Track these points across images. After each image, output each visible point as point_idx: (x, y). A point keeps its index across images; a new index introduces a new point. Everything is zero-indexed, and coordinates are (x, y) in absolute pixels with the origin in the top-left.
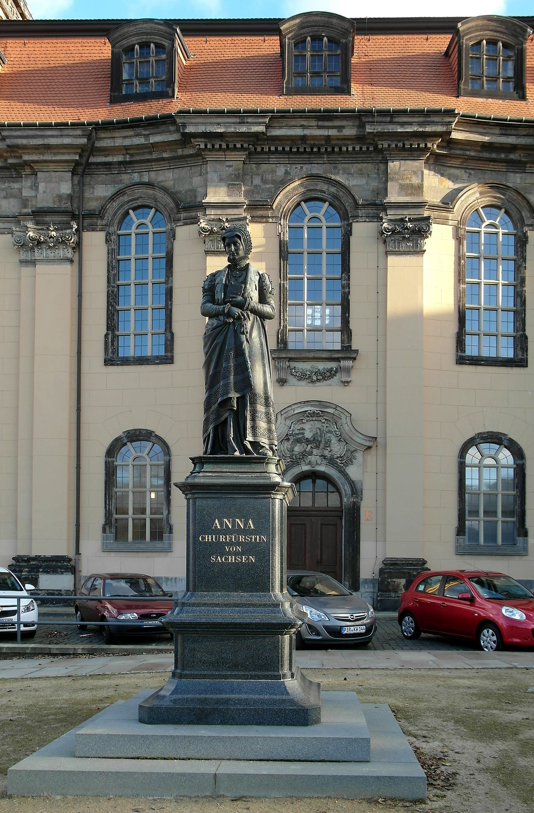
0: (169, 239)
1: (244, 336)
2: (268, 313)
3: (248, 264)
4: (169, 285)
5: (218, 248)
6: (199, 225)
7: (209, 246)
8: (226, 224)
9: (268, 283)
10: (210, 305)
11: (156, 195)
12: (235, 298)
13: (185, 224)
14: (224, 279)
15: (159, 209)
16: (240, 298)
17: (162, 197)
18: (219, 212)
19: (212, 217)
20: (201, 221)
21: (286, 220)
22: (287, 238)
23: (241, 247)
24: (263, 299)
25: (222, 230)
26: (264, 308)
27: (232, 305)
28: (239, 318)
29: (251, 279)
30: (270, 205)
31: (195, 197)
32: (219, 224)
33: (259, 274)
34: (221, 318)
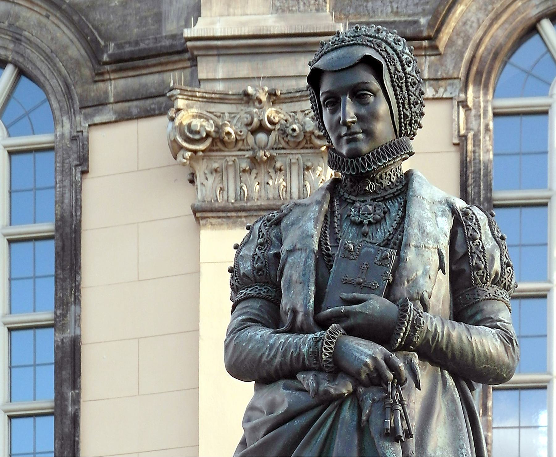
0: (65, 172)
1: (398, 447)
2: (489, 358)
3: (409, 175)
4: (69, 334)
5: (240, 196)
6: (172, 119)
7: (208, 189)
8: (270, 112)
9: (489, 243)
11: (17, 17)
12: (359, 301)
13: (124, 117)
15: (29, 67)
16: (377, 304)
17: (40, 25)
18: (243, 68)
19: (220, 87)
20: (181, 103)
21: (486, 87)
22: (486, 153)
23: (383, 108)
24: (465, 306)
25: (254, 132)
27: (350, 331)
28: (376, 379)
29: (423, 231)
30: (429, 38)
31: (159, 18)
32: (244, 113)
33: (454, 211)
34: (308, 380)
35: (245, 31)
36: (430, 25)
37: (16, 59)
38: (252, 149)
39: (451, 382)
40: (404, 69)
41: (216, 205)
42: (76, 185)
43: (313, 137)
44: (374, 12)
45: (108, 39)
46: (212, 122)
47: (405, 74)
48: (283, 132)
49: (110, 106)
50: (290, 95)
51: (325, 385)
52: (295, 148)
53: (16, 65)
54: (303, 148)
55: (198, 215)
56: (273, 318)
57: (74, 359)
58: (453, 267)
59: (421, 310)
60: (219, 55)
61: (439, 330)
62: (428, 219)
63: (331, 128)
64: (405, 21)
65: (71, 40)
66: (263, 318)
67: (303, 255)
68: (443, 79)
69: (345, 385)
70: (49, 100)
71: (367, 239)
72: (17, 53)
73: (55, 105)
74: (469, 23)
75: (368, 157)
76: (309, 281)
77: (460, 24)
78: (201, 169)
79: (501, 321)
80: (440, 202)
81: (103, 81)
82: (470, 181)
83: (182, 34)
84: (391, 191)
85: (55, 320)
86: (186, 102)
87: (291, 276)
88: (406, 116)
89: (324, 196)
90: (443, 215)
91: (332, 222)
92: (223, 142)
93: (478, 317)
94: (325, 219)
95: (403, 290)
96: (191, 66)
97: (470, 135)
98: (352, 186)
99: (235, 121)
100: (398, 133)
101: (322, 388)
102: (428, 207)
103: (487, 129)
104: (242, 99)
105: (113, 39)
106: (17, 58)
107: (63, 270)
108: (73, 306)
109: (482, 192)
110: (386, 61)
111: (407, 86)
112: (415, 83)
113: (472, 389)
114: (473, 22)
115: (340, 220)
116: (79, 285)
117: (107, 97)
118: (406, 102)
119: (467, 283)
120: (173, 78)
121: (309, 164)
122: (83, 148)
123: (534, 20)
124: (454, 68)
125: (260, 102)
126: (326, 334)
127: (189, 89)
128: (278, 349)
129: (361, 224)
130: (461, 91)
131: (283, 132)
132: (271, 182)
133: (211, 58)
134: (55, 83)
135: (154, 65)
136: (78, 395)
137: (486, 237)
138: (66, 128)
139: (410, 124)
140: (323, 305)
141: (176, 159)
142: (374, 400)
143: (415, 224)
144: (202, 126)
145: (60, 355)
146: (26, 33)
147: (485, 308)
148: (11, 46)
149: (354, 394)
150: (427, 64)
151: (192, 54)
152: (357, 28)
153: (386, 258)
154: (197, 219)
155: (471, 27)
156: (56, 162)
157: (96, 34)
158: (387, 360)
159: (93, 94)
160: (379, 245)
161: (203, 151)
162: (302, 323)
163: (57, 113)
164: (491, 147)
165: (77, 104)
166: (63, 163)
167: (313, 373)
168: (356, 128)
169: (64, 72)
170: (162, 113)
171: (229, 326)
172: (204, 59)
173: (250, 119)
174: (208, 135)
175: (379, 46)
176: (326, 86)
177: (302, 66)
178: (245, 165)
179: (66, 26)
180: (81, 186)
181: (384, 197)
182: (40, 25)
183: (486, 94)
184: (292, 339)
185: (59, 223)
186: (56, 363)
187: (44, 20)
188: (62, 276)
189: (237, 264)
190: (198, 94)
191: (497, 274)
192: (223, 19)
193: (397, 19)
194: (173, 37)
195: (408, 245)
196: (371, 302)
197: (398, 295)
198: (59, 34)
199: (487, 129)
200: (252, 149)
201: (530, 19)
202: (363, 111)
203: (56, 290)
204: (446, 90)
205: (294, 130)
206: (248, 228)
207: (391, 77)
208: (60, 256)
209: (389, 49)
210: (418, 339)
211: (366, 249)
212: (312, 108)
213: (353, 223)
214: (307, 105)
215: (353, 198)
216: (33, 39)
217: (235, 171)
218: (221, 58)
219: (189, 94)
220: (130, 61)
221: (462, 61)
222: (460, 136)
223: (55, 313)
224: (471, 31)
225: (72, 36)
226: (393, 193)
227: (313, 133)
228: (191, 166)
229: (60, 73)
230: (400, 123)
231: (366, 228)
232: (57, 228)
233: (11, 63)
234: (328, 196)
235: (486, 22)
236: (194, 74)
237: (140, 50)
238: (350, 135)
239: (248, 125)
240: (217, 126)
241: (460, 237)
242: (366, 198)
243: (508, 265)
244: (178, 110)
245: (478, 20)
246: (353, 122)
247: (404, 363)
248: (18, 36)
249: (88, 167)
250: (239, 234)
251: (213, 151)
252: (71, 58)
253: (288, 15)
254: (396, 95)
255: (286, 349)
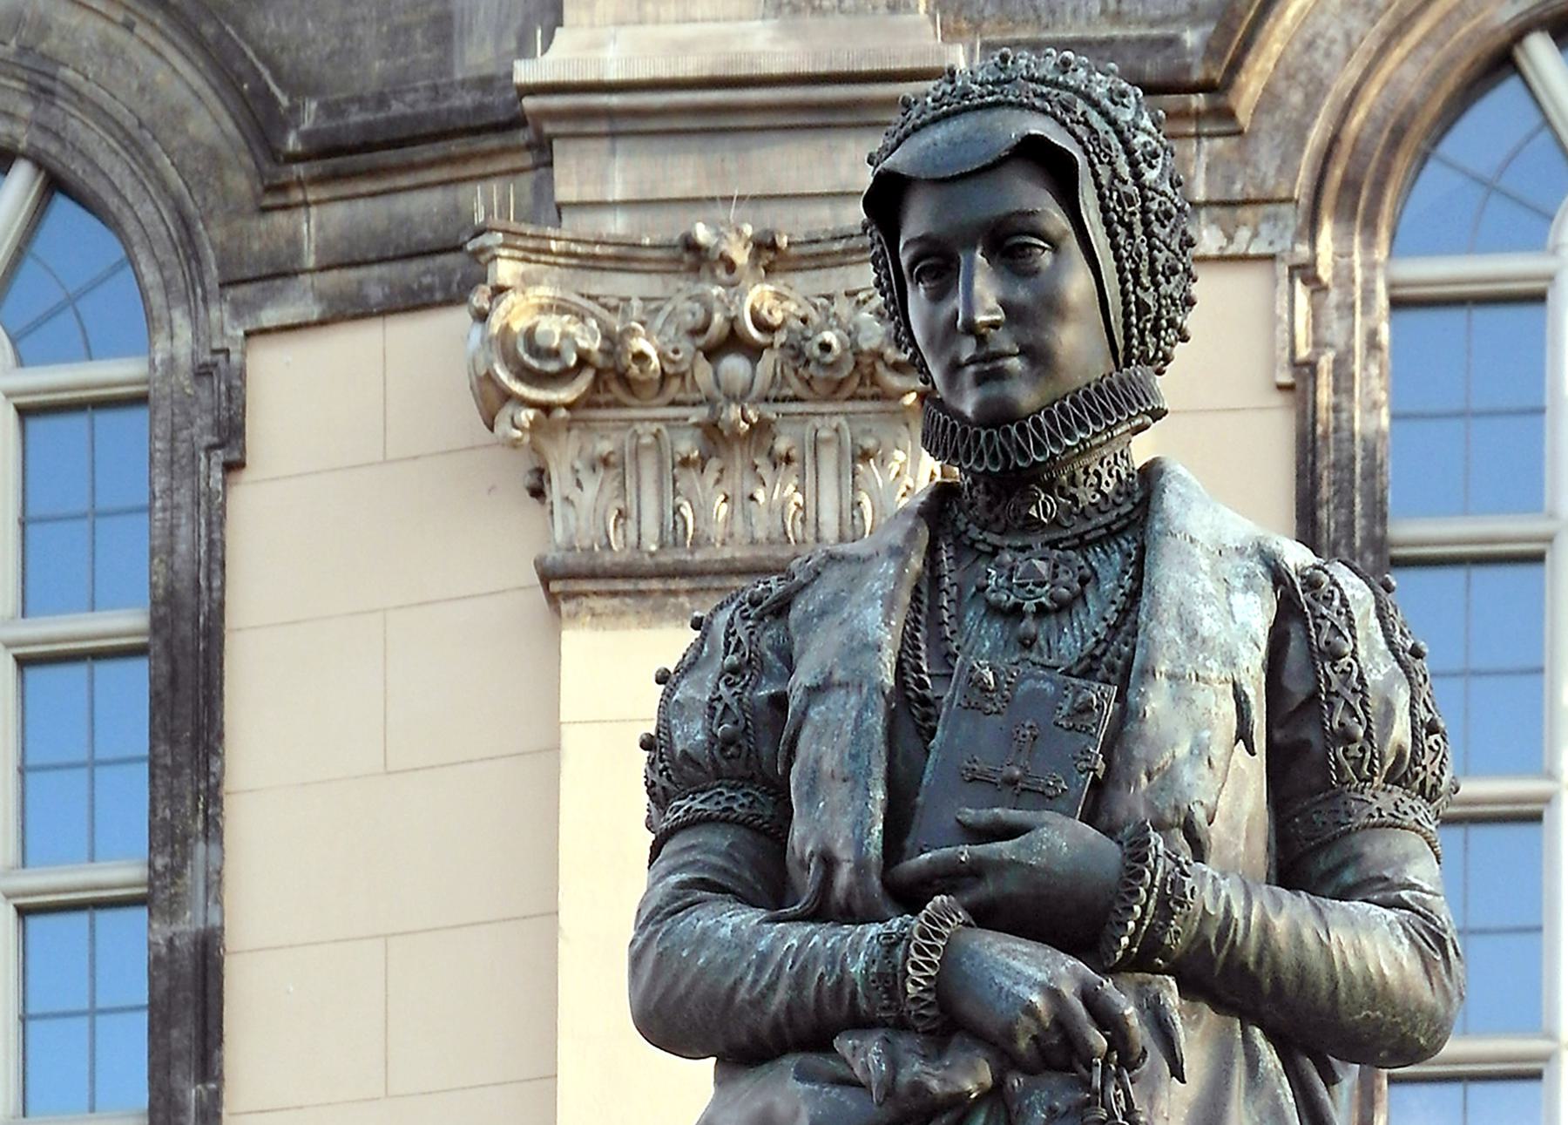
0: (179, 464)
2: (1378, 993)
3: (1151, 475)
4: (189, 923)
5: (672, 534)
6: (482, 316)
7: (583, 513)
9: (1379, 668)
10: (734, 921)
13: (346, 311)
14: (889, 639)
15: (76, 169)
16: (1061, 840)
17: (108, 51)
18: (681, 171)
19: (616, 225)
20: (506, 270)
21: (1370, 225)
23: (1077, 284)
24: (1311, 848)
25: (713, 353)
26: (1340, 937)
27: (986, 916)
28: (1059, 1051)
29: (1191, 634)
30: (1207, 87)
32: (684, 297)
33: (1278, 576)
34: (865, 1054)
35: (688, 67)
36: (1212, 51)
37: (40, 144)
38: (709, 401)
39: (1270, 1058)
40: (1137, 176)
41: (607, 559)
42: (210, 502)
43: (880, 367)
44: (1052, 12)
45: (300, 88)
46: (593, 323)
47: (1142, 187)
48: (796, 352)
49: (306, 280)
50: (815, 248)
51: (914, 1068)
52: (831, 397)
53: (39, 163)
54: (851, 398)
55: (555, 587)
56: (766, 878)
57: (205, 994)
58: (1278, 735)
59: (1186, 856)
60: (613, 135)
61: (1237, 913)
62: (1207, 599)
63: (930, 341)
64: (1141, 40)
65: (195, 93)
66: (739, 878)
67: (853, 699)
68: (1247, 202)
69: (971, 1069)
70: (132, 261)
71: (1034, 656)
72: (44, 128)
73: (151, 277)
74: (1322, 43)
75: (1036, 423)
76: (869, 774)
77: (1298, 46)
78: (563, 458)
79: (1412, 886)
80: (1240, 551)
81: (285, 207)
82: (1325, 491)
83: (510, 75)
84: (1102, 520)
85: (150, 884)
86: (522, 267)
87: (818, 761)
88: (1143, 308)
89: (911, 534)
90: (1247, 588)
91: (935, 607)
92: (624, 380)
93: (1349, 877)
94: (916, 598)
95: (1135, 799)
96: (536, 167)
97: (1325, 362)
98: (990, 507)
99: (659, 322)
100: (1122, 356)
101: (904, 1077)
102: (1205, 563)
103: (1373, 344)
104: (679, 260)
105: (314, 90)
106: (41, 143)
107: (173, 742)
108: (201, 845)
109: (1359, 523)
110: (1086, 152)
111: (1146, 224)
112: (1168, 215)
113: (1330, 1079)
114: (1333, 41)
115: (957, 601)
116: (219, 784)
117: (298, 254)
118: (1144, 266)
119: (1316, 781)
120: (483, 200)
121: (869, 443)
122: (230, 399)
123: (1504, 36)
124: (1280, 170)
125: (731, 266)
126: (917, 923)
127: (529, 230)
128: (781, 966)
129: (1016, 612)
130: (1298, 236)
131: (796, 352)
132: (760, 495)
133: (590, 144)
134: (149, 213)
135: (430, 164)
136: (216, 1097)
137: (1371, 648)
138: (181, 342)
139: (1156, 331)
140: (908, 843)
141: (492, 429)
142: (1052, 1111)
143: (1168, 613)
144: (565, 335)
145: (164, 982)
146: (69, 74)
147: (1367, 849)
148: (26, 109)
149: (995, 1093)
150: (1204, 159)
151: (539, 132)
152: (1004, 58)
153: (1087, 708)
154: (552, 598)
155: (1328, 54)
156: (152, 438)
157: (266, 74)
158: (1090, 998)
159: (256, 246)
160: (1068, 673)
161: (569, 407)
162: (850, 894)
163: (157, 299)
164: (1383, 396)
165: (213, 274)
166: (173, 439)
167: (881, 1033)
168: (1003, 341)
169: (175, 181)
170: (454, 299)
171: (644, 902)
172: (573, 147)
173: (700, 316)
174: (583, 361)
175: (1066, 109)
176: (916, 223)
177: (850, 164)
178: (687, 446)
179: (182, 52)
180: (223, 506)
181: (1081, 536)
182: (108, 51)
183: (1369, 245)
184: (822, 937)
185: (162, 610)
186: (153, 1006)
187: (119, 36)
188: (169, 761)
189: (664, 725)
190: (554, 246)
191: (1400, 754)
192: (625, 32)
193: (1117, 32)
194: (485, 83)
195: (1148, 672)
196: (1045, 833)
197: (1122, 813)
198: (161, 76)
199: (1373, 344)
200: (709, 401)
201: (1495, 32)
202: (1022, 294)
203: (153, 800)
204: (1255, 235)
205: (826, 347)
206: (697, 624)
207: (1101, 197)
208: (162, 702)
209: (1094, 118)
210: (1176, 938)
211: (1030, 683)
212: (878, 284)
213: (995, 610)
214: (865, 276)
215: (994, 539)
216: (86, 88)
217: (661, 462)
218: (621, 144)
219: (531, 244)
220: (361, 152)
221: (1301, 151)
222: (1295, 365)
223: (151, 865)
224: (1327, 66)
225: (197, 82)
226: (1107, 526)
227: (880, 355)
228: (535, 449)
229: (164, 186)
230: (1127, 326)
231: (1029, 625)
232: (156, 624)
233: (25, 156)
234: (924, 534)
235: (1371, 42)
236: (544, 188)
237: (390, 122)
238: (985, 360)
239: (697, 332)
240: (608, 336)
241: (1295, 648)
242: (1030, 540)
243: (1432, 728)
244: (499, 290)
245: (1348, 35)
246: (994, 325)
247: (1139, 1007)
248: (44, 82)
249: (243, 451)
250: (670, 642)
251: (598, 406)
252: (196, 144)
253: (809, 20)
254: (1115, 247)
255: (804, 968)
